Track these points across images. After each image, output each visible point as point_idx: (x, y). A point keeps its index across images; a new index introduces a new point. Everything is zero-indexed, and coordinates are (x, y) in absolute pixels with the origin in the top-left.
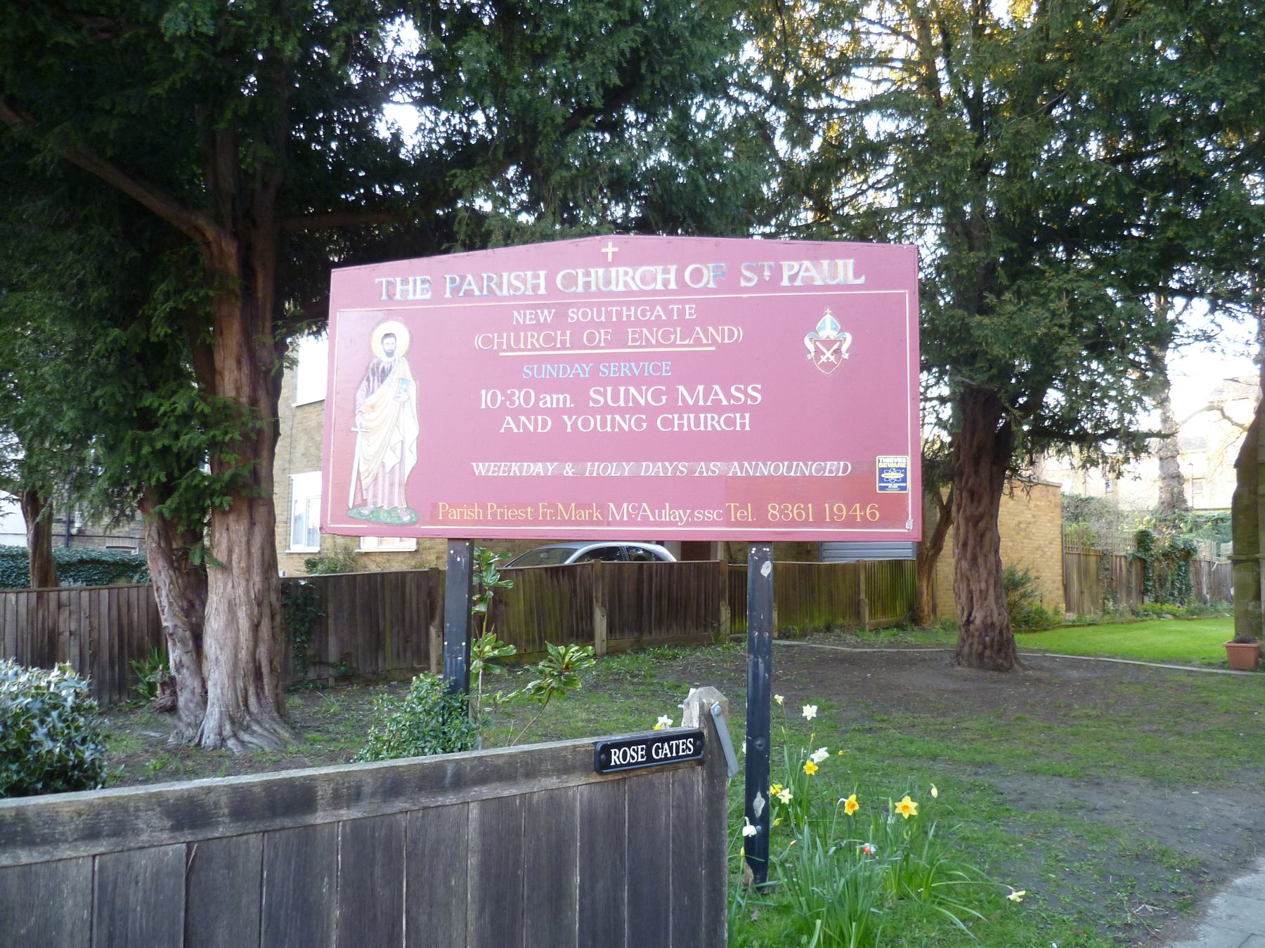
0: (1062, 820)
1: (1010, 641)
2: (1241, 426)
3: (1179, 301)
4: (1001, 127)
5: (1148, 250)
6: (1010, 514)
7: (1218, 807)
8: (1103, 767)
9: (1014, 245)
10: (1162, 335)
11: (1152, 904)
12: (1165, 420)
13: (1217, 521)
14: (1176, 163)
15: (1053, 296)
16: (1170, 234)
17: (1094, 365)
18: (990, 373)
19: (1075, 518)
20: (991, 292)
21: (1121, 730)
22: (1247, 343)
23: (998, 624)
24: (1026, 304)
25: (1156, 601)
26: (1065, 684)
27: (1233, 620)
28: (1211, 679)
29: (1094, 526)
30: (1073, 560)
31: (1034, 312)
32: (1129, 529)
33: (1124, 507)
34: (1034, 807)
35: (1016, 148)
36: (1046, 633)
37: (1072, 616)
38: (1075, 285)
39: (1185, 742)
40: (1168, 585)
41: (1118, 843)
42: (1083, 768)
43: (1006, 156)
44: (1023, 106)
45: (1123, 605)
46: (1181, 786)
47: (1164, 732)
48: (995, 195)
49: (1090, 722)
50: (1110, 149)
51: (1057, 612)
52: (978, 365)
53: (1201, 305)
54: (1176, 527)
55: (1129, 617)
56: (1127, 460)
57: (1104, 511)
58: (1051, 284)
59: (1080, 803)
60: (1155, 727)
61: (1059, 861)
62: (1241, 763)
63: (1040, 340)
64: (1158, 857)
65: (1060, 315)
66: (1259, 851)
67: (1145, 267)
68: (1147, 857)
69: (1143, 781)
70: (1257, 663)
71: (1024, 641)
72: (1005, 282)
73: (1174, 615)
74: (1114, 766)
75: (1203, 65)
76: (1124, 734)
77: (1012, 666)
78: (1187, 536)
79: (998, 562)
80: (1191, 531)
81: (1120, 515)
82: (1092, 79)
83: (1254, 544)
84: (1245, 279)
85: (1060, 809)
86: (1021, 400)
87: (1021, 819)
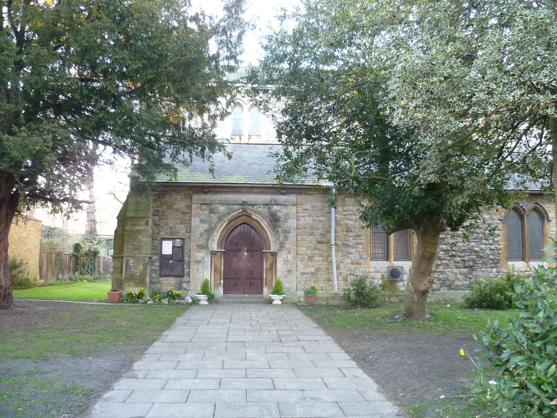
0: (28, 380)
1: (10, 294)
2: (121, 202)
3: (101, 146)
4: (31, 49)
5: (91, 121)
6: (16, 233)
7: (99, 363)
8: (50, 351)
9: (30, 105)
10: (93, 159)
11: (68, 414)
12: (91, 196)
13: (108, 241)
14: (107, 87)
15: (45, 132)
16: (101, 116)
17: (62, 168)
18: (11, 164)
19: (48, 236)
20: (16, 125)
21: (60, 333)
22: (126, 168)
23: (4, 286)
24: (32, 134)
25: (81, 274)
26: (35, 314)
27: (111, 282)
28: (101, 307)
29: (56, 240)
30: (45, 255)
31: (35, 138)
32: (71, 243)
33: (70, 233)
34: (14, 376)
35: (37, 61)
36: (30, 289)
37: (42, 281)
38: (56, 130)
39: (87, 336)
40: (86, 267)
41: (54, 387)
42: (41, 353)
43: (31, 63)
44: (43, 43)
45: (66, 276)
46: (84, 356)
47: (79, 332)
48: (25, 81)
49: (45, 331)
50: (80, 74)
51: (35, 280)
52: (4, 159)
53: (110, 149)
54: (91, 242)
55: (68, 281)
56: (72, 212)
57: (63, 235)
58: (45, 127)
59: (37, 370)
60: (75, 331)
61: (24, 401)
62: (110, 343)
63: (37, 152)
64: (72, 391)
65: (48, 142)
66: (115, 380)
67: (88, 128)
68: (67, 392)
69: (67, 356)
70: (119, 299)
71: (17, 294)
72: (24, 122)
73: (88, 280)
74: (55, 351)
75: (123, 50)
76: (61, 335)
77: (10, 306)
78: (96, 246)
79: (7, 256)
80: (97, 244)
81: (68, 236)
82: (76, 40)
83: (122, 251)
84: (128, 141)
85: (27, 375)
86: (26, 179)
87: (7, 382)
